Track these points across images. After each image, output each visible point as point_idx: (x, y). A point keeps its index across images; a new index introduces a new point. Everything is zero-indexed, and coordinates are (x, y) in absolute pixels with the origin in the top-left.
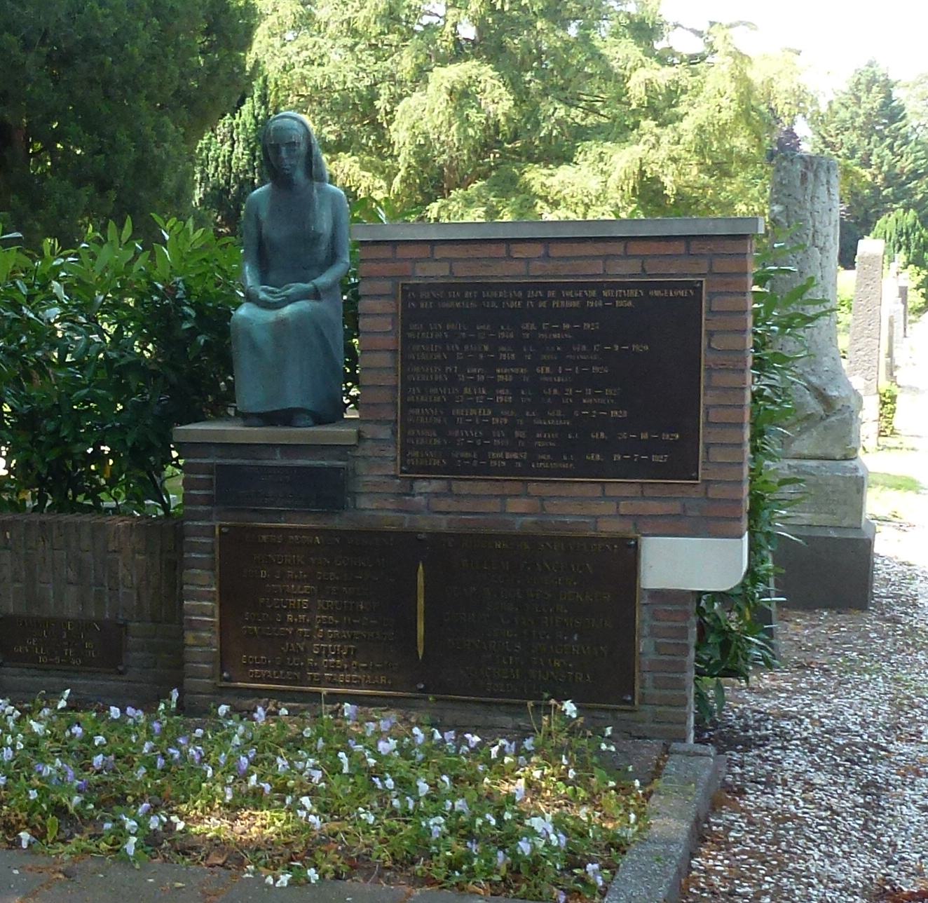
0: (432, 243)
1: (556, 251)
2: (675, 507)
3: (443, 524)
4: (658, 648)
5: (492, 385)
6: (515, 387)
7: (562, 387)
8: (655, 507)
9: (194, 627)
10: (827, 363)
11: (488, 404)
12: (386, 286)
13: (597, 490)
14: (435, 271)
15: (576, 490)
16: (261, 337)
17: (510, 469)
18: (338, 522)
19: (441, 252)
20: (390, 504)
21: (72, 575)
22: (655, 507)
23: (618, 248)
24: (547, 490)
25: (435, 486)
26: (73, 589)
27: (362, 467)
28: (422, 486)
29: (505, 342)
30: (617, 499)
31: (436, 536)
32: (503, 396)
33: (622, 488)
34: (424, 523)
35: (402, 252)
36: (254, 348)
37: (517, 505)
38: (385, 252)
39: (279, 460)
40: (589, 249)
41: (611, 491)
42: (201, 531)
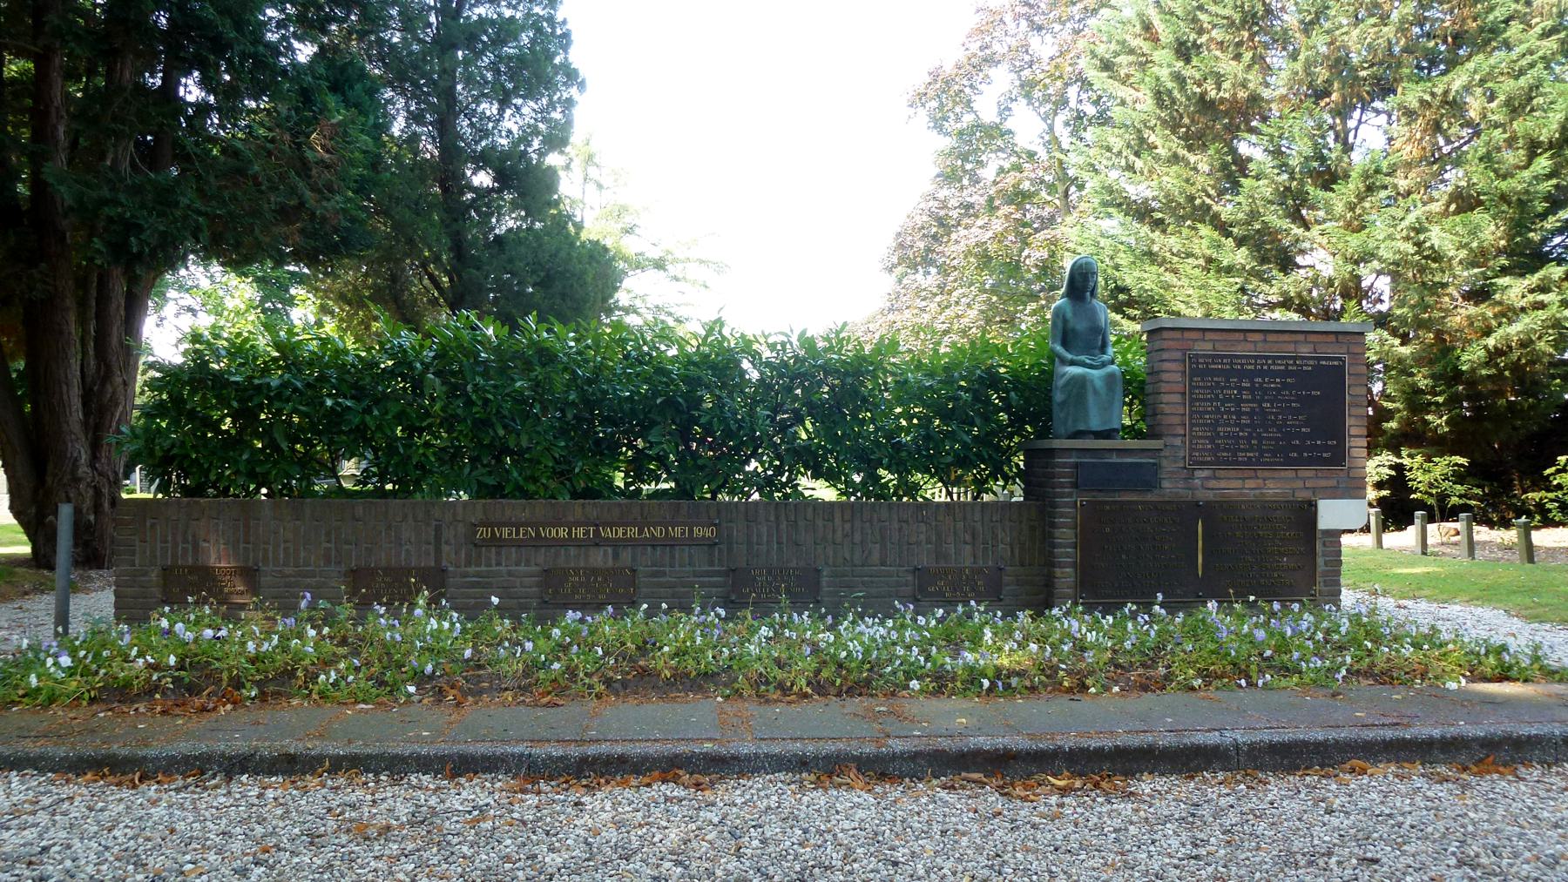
0: (1204, 330)
1: (1270, 338)
2: (1333, 483)
3: (1210, 495)
4: (1326, 564)
5: (1239, 414)
6: (1251, 414)
7: (1276, 414)
8: (1323, 483)
9: (1061, 565)
10: (615, 362)
11: (1237, 425)
12: (1178, 355)
13: (1293, 474)
14: (1204, 348)
15: (1283, 474)
16: (1099, 384)
17: (1249, 462)
18: (1149, 497)
19: (1209, 336)
20: (1181, 484)
21: (968, 538)
22: (1323, 483)
23: (1301, 337)
24: (1267, 474)
25: (1206, 473)
26: (968, 547)
27: (1164, 463)
28: (1198, 474)
29: (1246, 389)
30: (1304, 479)
31: (1208, 503)
32: (1245, 420)
33: (1307, 472)
34: (1203, 496)
35: (1187, 335)
36: (1096, 392)
37: (1250, 484)
38: (1178, 335)
39: (1115, 459)
40: (1286, 337)
41: (1300, 474)
42: (1066, 505)
